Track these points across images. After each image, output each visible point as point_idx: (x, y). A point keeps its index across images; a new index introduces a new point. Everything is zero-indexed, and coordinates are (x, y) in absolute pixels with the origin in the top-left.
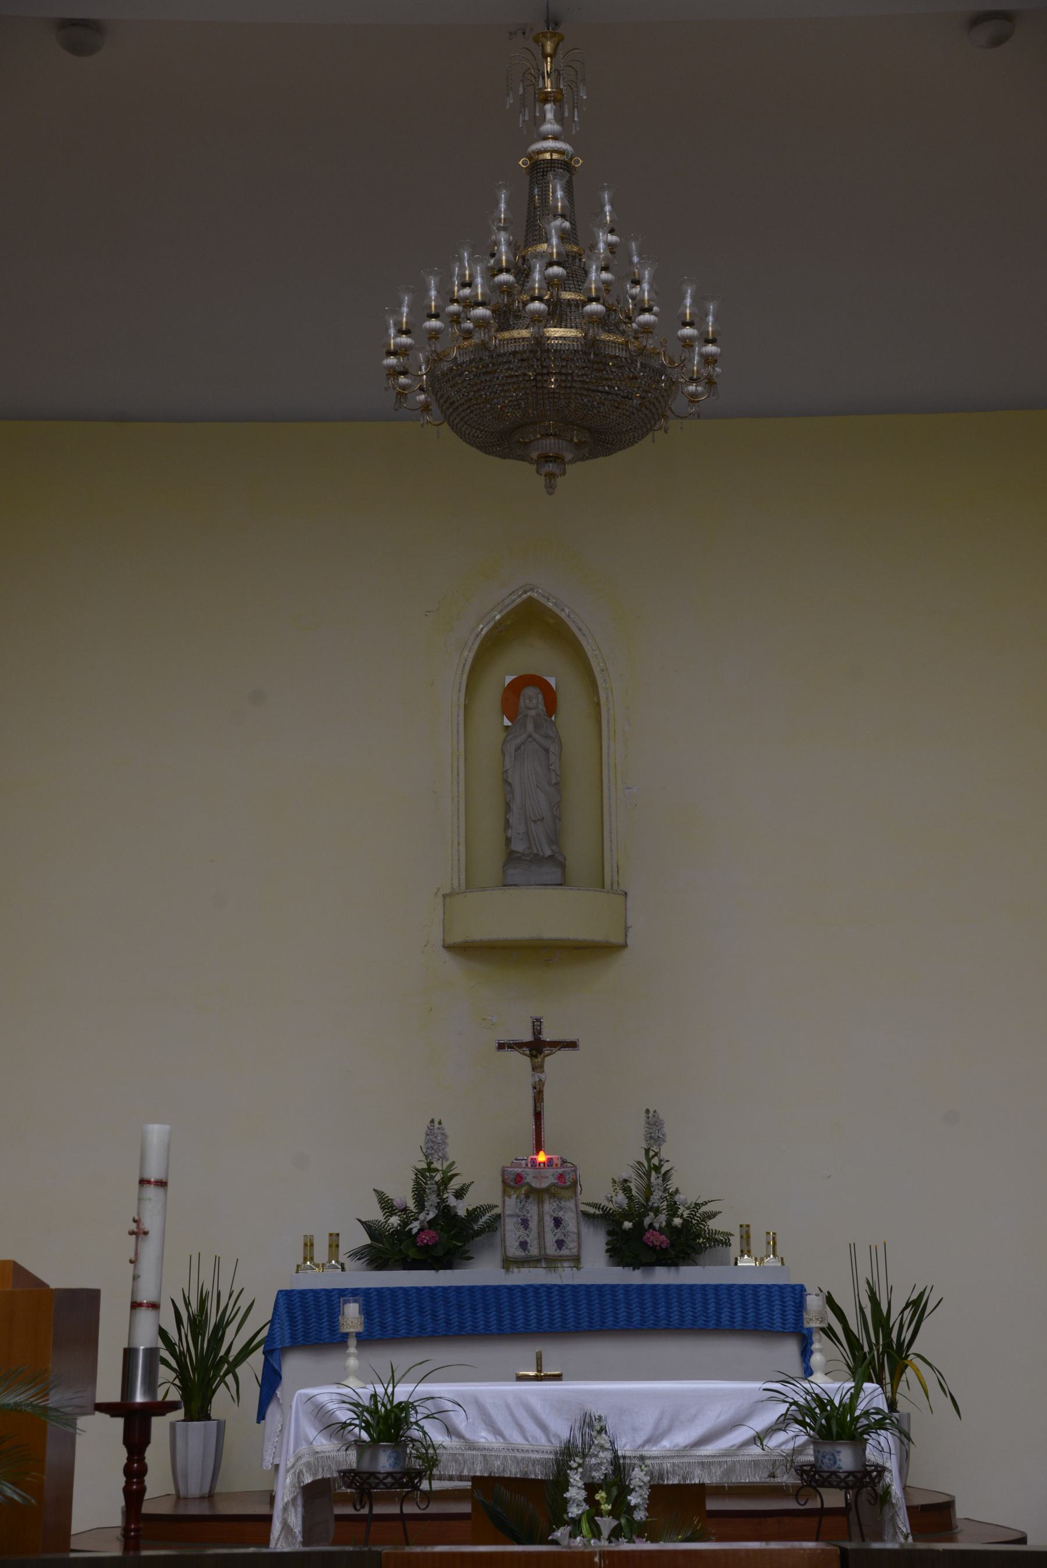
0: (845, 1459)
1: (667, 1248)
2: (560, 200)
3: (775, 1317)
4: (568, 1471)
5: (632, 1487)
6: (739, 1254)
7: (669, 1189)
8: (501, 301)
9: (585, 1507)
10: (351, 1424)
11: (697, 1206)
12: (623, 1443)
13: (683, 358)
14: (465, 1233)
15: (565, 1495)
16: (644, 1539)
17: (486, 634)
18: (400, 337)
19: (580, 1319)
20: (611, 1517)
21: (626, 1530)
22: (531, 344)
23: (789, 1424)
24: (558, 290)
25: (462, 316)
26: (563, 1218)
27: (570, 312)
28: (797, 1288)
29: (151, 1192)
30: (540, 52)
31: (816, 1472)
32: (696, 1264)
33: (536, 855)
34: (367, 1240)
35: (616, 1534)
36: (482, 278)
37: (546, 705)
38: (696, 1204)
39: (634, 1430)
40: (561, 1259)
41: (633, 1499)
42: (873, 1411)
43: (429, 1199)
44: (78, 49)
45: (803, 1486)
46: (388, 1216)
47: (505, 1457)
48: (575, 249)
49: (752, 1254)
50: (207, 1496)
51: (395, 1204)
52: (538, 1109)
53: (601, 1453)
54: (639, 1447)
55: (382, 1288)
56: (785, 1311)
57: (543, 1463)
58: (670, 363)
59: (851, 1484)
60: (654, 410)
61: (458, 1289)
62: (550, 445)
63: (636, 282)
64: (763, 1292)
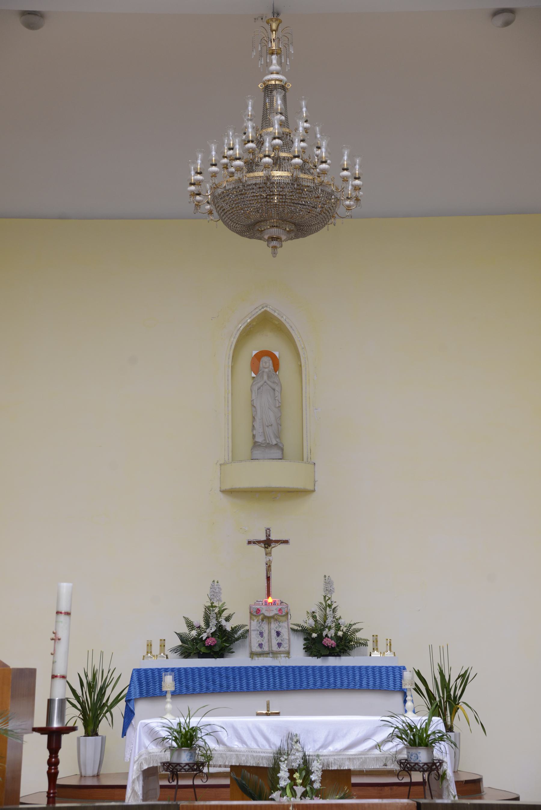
0: (422, 756)
1: (335, 647)
2: (279, 105)
3: (390, 683)
4: (280, 763)
5: (312, 771)
6: (372, 650)
7: (336, 616)
8: (249, 157)
9: (289, 781)
10: (167, 738)
11: (351, 625)
12: (309, 748)
13: (343, 187)
14: (230, 639)
15: (278, 775)
16: (319, 798)
17: (243, 329)
18: (197, 175)
19: (289, 684)
20: (302, 786)
21: (310, 793)
22: (264, 180)
23: (393, 738)
24: (278, 152)
25: (229, 165)
26: (281, 631)
27: (285, 163)
28: (402, 668)
29: (62, 617)
30: (270, 28)
31: (408, 763)
32: (349, 655)
33: (268, 444)
34: (180, 643)
35: (304, 795)
36: (239, 145)
37: (274, 366)
38: (350, 624)
39: (314, 741)
40: (280, 653)
41: (313, 777)
42: (437, 731)
43: (212, 622)
44: (31, 26)
45: (401, 771)
46: (191, 630)
47: (247, 755)
48: (288, 130)
49: (379, 650)
50: (96, 775)
51: (194, 624)
52: (269, 575)
53: (297, 753)
54: (317, 750)
55: (187, 668)
56: (395, 680)
57: (267, 758)
58: (336, 189)
59: (425, 769)
60: (328, 214)
61: (227, 668)
62: (275, 232)
63: (319, 148)
64: (384, 670)
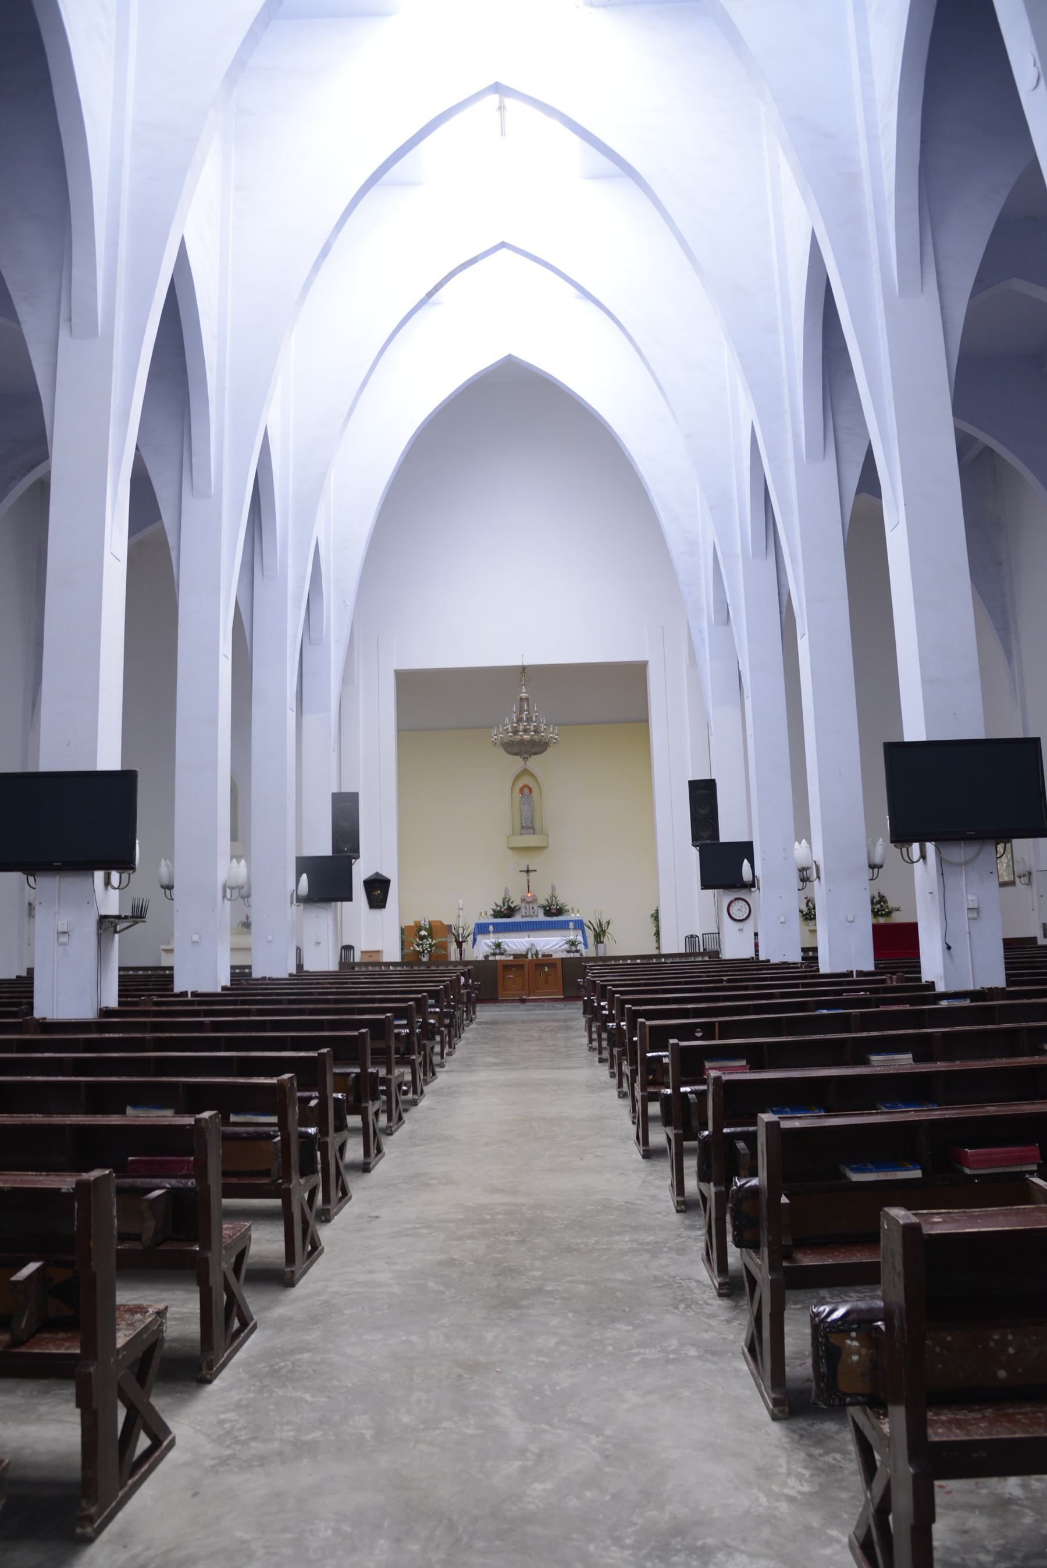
29: (461, 910)
34: (493, 913)
61: (512, 923)
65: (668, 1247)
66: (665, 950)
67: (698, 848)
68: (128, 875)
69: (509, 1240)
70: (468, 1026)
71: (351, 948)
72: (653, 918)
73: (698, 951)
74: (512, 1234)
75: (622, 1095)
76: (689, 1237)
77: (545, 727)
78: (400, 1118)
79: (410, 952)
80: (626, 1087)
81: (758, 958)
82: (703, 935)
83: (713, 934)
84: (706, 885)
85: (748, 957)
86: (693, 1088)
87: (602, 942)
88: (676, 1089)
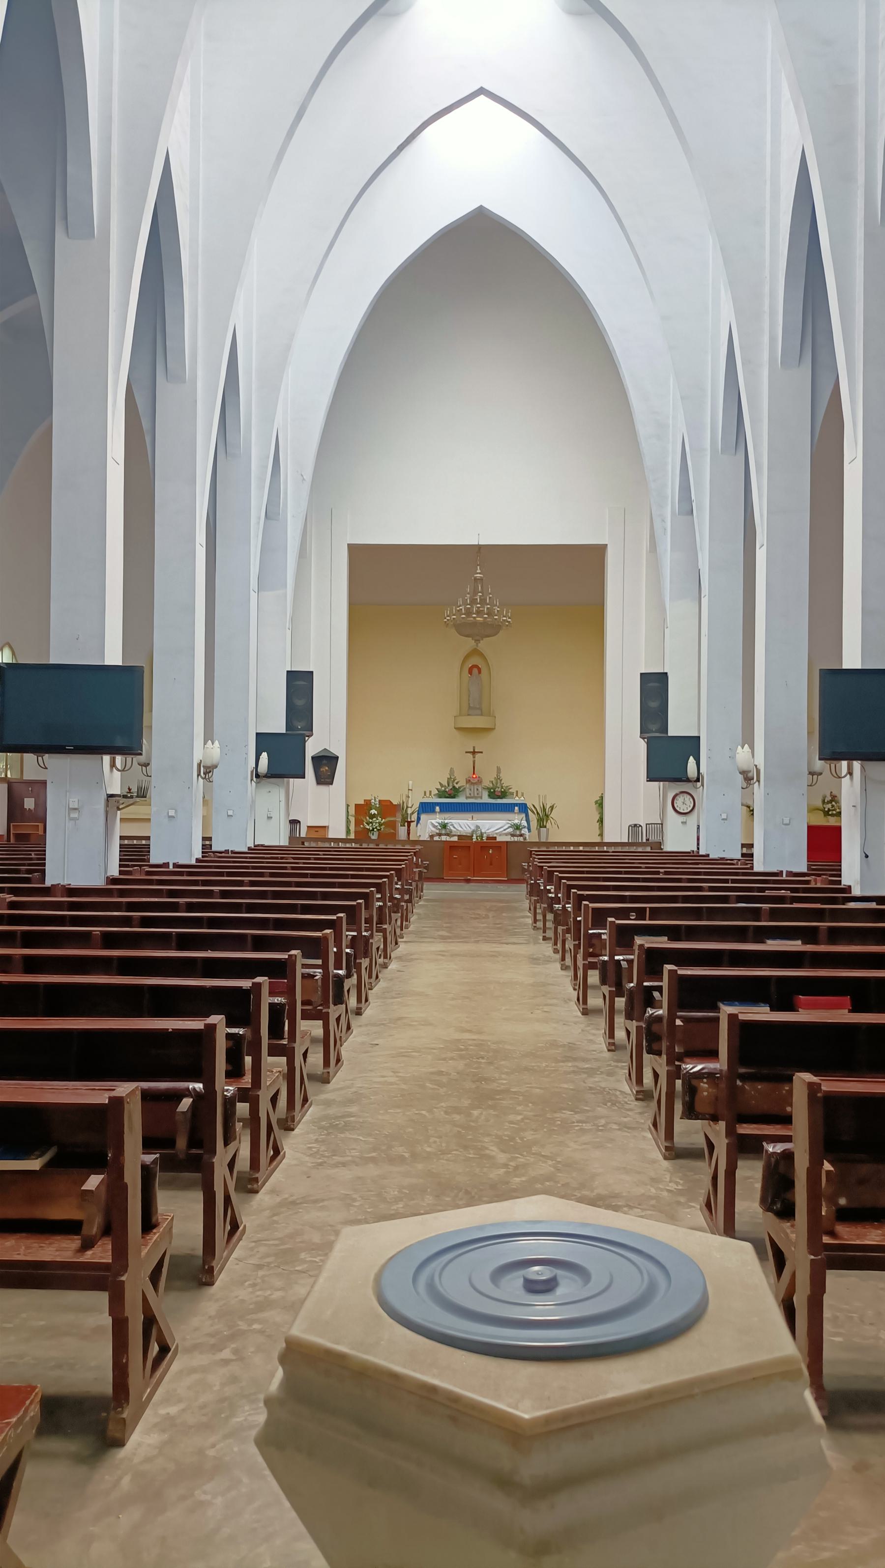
11: (507, 787)
29: (410, 791)
65: (600, 1072)
66: (607, 839)
67: (646, 740)
68: (131, 759)
69: (481, 1062)
70: (418, 903)
71: (297, 823)
72: (597, 805)
73: (640, 841)
74: (483, 1058)
75: (564, 968)
76: (617, 1067)
77: (498, 609)
78: (377, 977)
79: (361, 829)
80: (568, 961)
81: (698, 852)
82: (647, 824)
83: (654, 824)
84: (650, 778)
85: (689, 850)
86: (625, 957)
87: (545, 827)
88: (612, 956)
